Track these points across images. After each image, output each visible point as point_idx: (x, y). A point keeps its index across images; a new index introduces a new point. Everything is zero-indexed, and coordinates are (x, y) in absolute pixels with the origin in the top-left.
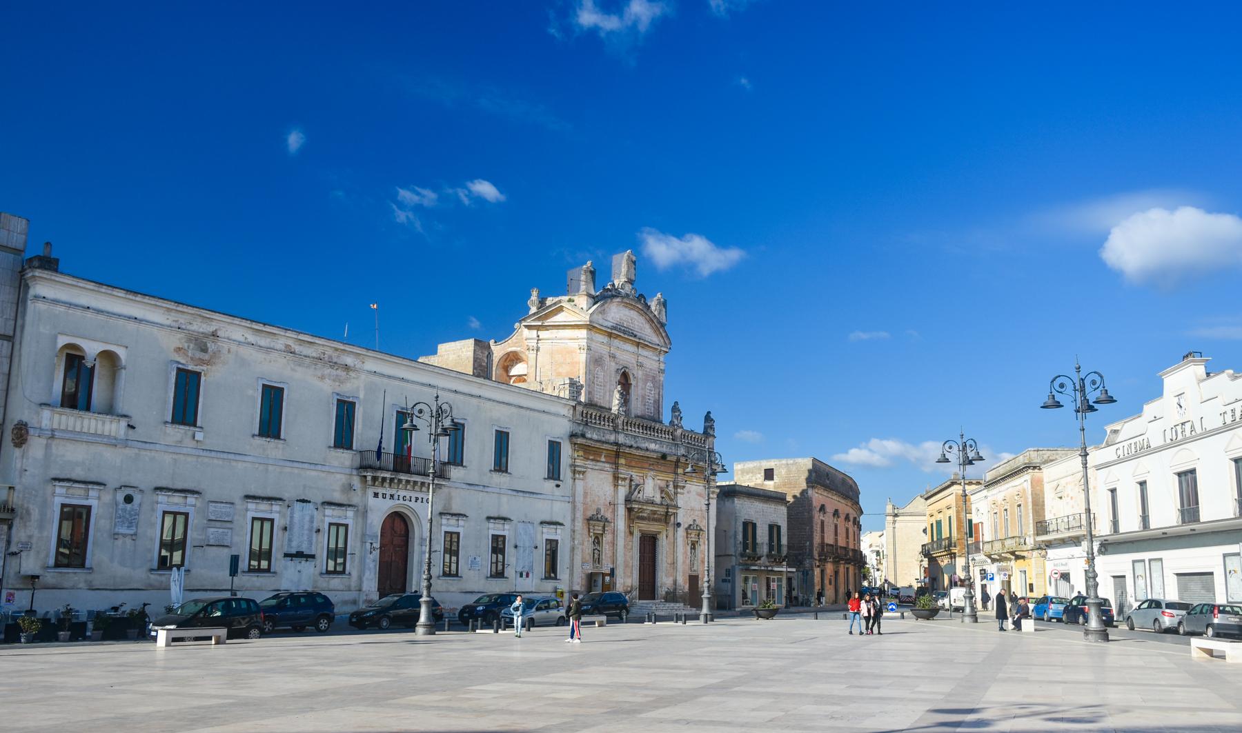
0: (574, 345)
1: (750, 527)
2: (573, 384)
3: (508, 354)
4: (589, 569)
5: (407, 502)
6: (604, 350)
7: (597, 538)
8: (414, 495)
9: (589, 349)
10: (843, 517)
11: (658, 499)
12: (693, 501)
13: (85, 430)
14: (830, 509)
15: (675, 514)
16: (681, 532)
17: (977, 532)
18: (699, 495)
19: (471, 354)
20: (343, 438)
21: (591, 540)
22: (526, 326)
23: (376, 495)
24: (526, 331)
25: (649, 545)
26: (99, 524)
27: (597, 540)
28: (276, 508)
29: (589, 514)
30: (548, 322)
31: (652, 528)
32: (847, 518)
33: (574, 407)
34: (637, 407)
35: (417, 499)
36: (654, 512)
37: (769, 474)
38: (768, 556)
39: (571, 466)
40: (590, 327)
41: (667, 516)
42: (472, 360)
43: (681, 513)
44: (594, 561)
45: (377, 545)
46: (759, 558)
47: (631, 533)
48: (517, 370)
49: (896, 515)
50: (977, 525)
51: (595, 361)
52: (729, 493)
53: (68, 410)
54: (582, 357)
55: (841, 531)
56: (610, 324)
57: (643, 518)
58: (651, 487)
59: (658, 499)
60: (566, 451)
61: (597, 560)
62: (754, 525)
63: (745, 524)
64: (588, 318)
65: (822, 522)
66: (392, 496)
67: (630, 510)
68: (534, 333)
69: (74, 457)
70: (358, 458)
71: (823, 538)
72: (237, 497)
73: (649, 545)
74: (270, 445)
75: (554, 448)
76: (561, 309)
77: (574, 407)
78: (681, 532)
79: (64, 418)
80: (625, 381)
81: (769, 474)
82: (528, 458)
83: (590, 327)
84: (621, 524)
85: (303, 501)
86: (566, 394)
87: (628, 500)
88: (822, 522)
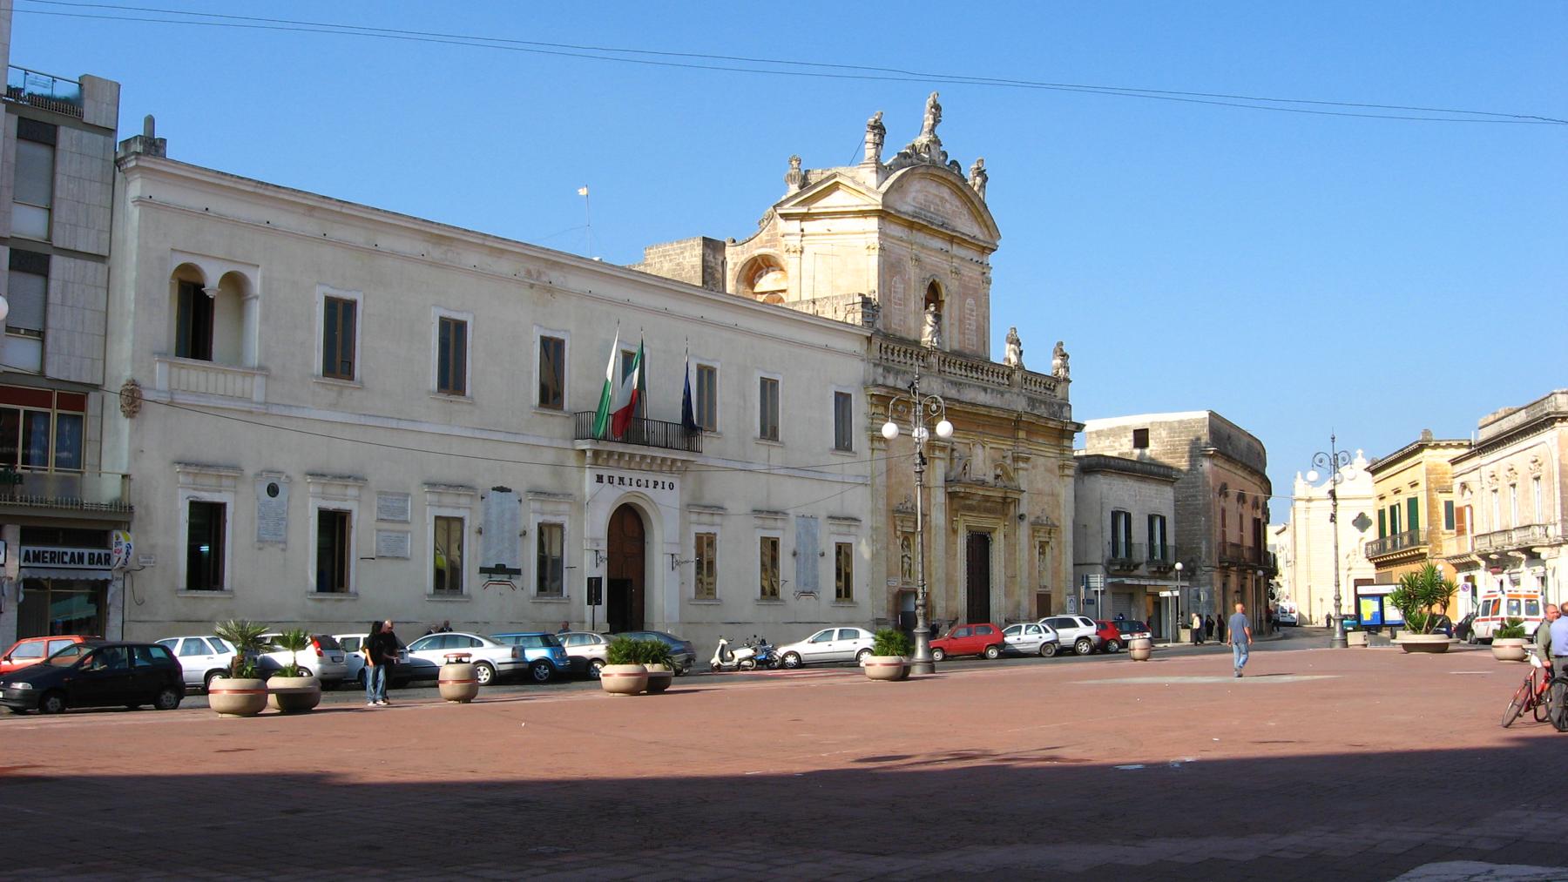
0: (861, 242)
1: (1120, 517)
2: (866, 302)
3: (755, 259)
4: (897, 583)
5: (642, 489)
6: (902, 251)
7: (906, 538)
8: (652, 478)
9: (882, 249)
10: (1250, 502)
11: (990, 479)
12: (1043, 485)
13: (211, 390)
14: (1233, 492)
15: (1016, 502)
16: (1024, 531)
17: (1461, 519)
18: (1050, 471)
19: (698, 261)
20: (551, 395)
21: (899, 542)
22: (782, 216)
23: (600, 479)
24: (781, 222)
25: (979, 546)
26: (362, 538)
27: (907, 538)
28: (564, 507)
29: (895, 502)
30: (817, 207)
31: (983, 522)
32: (1241, 498)
33: (869, 339)
34: (953, 342)
35: (656, 483)
36: (987, 498)
37: (1141, 438)
38: (1147, 563)
39: (867, 429)
40: (883, 214)
41: (1005, 504)
42: (699, 270)
43: (1024, 498)
44: (904, 575)
45: (604, 554)
46: (1137, 566)
47: (955, 531)
48: (767, 283)
49: (1310, 500)
50: (1461, 510)
51: (889, 267)
52: (1095, 466)
53: (190, 361)
54: (873, 261)
55: (1232, 522)
56: (910, 209)
57: (971, 508)
58: (982, 460)
59: (990, 479)
60: (860, 409)
61: (908, 572)
62: (1128, 517)
63: (1115, 515)
64: (879, 199)
65: (1223, 511)
66: (621, 479)
67: (951, 496)
68: (794, 226)
69: (208, 437)
70: (572, 423)
71: (1224, 533)
72: (823, 514)
73: (979, 546)
74: (456, 404)
75: (842, 400)
76: (835, 187)
77: (869, 339)
78: (1024, 531)
79: (184, 372)
80: (933, 295)
81: (1141, 438)
82: (805, 417)
83: (883, 214)
84: (939, 517)
85: (502, 489)
86: (857, 318)
87: (948, 481)
88: (1223, 511)
